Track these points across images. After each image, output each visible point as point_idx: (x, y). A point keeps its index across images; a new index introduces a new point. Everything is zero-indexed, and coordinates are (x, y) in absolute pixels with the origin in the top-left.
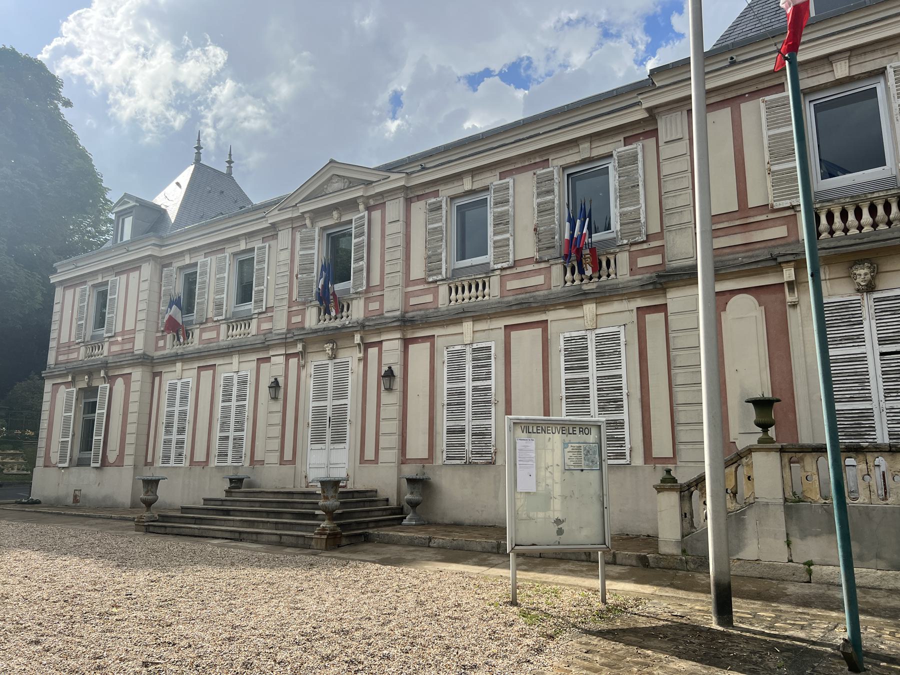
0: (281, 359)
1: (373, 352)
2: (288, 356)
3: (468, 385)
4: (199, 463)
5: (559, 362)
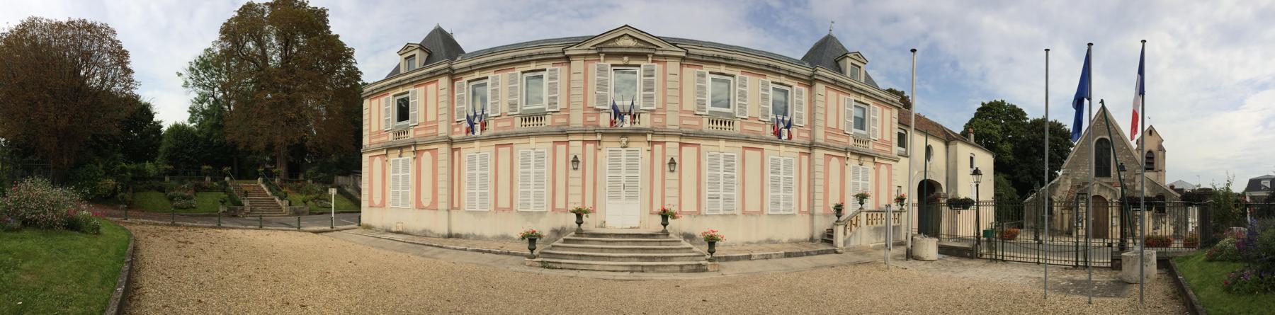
0: (580, 143)
1: (658, 148)
2: (585, 142)
3: (532, 170)
4: (752, 214)
5: (768, 168)
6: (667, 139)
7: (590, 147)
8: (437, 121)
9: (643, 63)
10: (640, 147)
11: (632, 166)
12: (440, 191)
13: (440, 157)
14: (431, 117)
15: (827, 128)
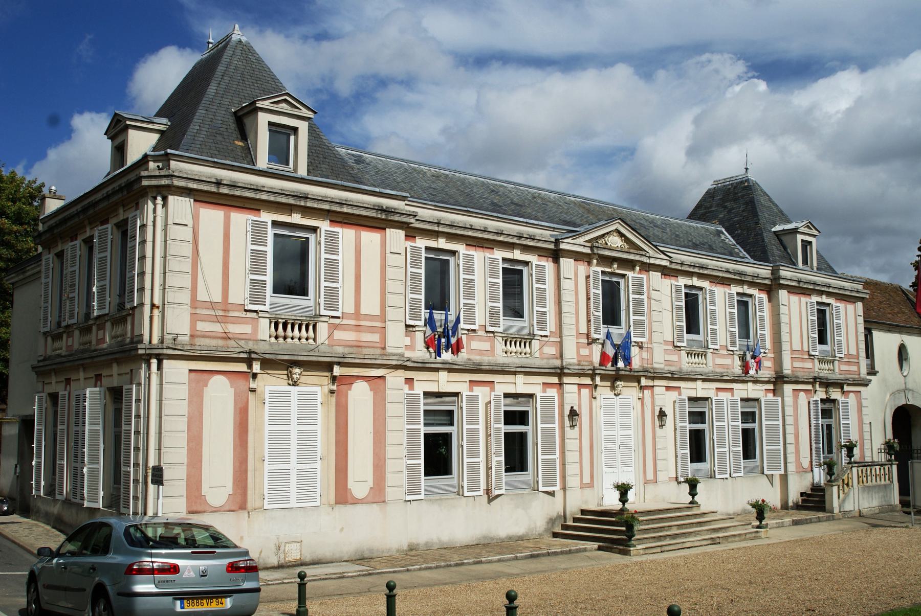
1: (647, 392)
6: (657, 382)
7: (585, 392)
8: (383, 317)
9: (630, 274)
10: (630, 392)
11: (625, 414)
12: (390, 466)
13: (390, 395)
14: (370, 306)
15: (793, 351)
